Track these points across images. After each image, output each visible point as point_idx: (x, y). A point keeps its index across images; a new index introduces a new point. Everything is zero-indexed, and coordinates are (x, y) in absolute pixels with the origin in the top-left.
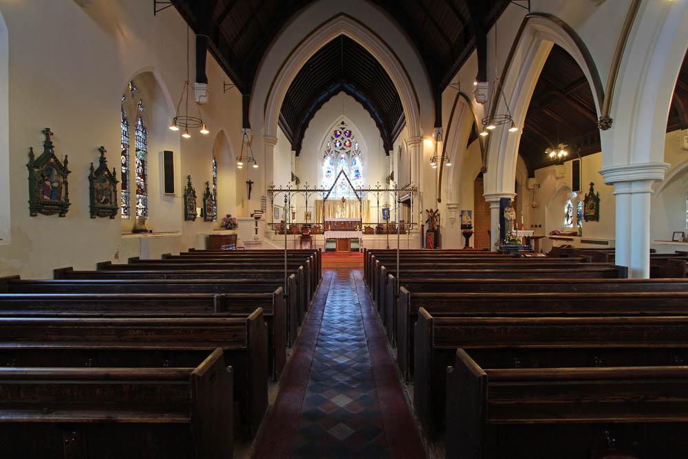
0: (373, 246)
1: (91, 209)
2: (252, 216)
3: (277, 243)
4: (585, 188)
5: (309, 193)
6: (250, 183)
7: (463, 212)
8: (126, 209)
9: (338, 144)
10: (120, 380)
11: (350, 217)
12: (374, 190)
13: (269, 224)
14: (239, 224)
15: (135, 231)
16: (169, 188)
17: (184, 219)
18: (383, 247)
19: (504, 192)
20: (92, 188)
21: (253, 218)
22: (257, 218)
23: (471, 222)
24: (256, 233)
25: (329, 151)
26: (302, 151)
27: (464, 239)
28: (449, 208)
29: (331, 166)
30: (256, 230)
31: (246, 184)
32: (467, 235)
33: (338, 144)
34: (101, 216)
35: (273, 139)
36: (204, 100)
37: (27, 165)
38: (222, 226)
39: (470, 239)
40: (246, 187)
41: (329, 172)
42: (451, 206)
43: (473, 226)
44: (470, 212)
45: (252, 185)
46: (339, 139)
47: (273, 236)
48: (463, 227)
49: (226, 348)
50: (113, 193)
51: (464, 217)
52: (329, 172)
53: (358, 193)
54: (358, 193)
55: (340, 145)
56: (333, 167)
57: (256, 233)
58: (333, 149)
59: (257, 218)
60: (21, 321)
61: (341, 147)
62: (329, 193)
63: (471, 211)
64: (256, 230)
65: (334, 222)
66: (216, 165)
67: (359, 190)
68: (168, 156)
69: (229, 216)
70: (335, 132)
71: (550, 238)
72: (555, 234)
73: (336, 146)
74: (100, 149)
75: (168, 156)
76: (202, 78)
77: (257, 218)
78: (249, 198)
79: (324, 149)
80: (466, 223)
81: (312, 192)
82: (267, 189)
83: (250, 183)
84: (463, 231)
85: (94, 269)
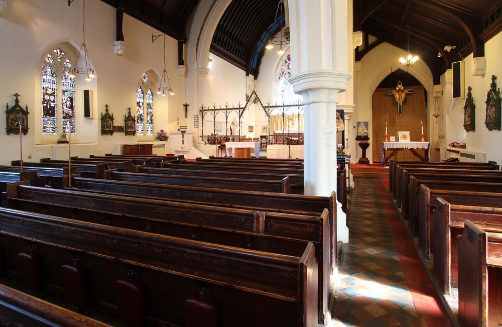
0: (278, 155)
1: (471, 130)
2: (179, 130)
4: (464, 92)
5: (228, 111)
6: (186, 106)
7: (359, 123)
8: (54, 128)
14: (170, 137)
15: (59, 142)
16: (87, 114)
17: (101, 134)
18: (286, 157)
20: (8, 118)
21: (180, 132)
22: (183, 132)
23: (367, 133)
24: (183, 143)
25: (283, 73)
26: (260, 76)
27: (361, 150)
29: (284, 86)
30: (183, 140)
31: (183, 106)
32: (364, 147)
34: (106, 134)
35: (204, 70)
36: (120, 52)
38: (157, 139)
39: (367, 150)
40: (183, 108)
41: (283, 91)
43: (371, 136)
44: (366, 124)
45: (188, 107)
47: (202, 145)
48: (358, 138)
50: (25, 120)
51: (360, 128)
52: (283, 91)
53: (267, 109)
54: (267, 109)
57: (183, 143)
58: (286, 71)
59: (182, 132)
62: (244, 110)
63: (367, 122)
64: (183, 140)
65: (337, 158)
66: (152, 95)
67: (267, 107)
68: (86, 93)
69: (162, 131)
71: (448, 150)
72: (453, 146)
74: (15, 95)
75: (86, 93)
76: (120, 37)
77: (183, 132)
78: (186, 117)
79: (279, 71)
81: (230, 110)
83: (186, 106)
85: (9, 164)
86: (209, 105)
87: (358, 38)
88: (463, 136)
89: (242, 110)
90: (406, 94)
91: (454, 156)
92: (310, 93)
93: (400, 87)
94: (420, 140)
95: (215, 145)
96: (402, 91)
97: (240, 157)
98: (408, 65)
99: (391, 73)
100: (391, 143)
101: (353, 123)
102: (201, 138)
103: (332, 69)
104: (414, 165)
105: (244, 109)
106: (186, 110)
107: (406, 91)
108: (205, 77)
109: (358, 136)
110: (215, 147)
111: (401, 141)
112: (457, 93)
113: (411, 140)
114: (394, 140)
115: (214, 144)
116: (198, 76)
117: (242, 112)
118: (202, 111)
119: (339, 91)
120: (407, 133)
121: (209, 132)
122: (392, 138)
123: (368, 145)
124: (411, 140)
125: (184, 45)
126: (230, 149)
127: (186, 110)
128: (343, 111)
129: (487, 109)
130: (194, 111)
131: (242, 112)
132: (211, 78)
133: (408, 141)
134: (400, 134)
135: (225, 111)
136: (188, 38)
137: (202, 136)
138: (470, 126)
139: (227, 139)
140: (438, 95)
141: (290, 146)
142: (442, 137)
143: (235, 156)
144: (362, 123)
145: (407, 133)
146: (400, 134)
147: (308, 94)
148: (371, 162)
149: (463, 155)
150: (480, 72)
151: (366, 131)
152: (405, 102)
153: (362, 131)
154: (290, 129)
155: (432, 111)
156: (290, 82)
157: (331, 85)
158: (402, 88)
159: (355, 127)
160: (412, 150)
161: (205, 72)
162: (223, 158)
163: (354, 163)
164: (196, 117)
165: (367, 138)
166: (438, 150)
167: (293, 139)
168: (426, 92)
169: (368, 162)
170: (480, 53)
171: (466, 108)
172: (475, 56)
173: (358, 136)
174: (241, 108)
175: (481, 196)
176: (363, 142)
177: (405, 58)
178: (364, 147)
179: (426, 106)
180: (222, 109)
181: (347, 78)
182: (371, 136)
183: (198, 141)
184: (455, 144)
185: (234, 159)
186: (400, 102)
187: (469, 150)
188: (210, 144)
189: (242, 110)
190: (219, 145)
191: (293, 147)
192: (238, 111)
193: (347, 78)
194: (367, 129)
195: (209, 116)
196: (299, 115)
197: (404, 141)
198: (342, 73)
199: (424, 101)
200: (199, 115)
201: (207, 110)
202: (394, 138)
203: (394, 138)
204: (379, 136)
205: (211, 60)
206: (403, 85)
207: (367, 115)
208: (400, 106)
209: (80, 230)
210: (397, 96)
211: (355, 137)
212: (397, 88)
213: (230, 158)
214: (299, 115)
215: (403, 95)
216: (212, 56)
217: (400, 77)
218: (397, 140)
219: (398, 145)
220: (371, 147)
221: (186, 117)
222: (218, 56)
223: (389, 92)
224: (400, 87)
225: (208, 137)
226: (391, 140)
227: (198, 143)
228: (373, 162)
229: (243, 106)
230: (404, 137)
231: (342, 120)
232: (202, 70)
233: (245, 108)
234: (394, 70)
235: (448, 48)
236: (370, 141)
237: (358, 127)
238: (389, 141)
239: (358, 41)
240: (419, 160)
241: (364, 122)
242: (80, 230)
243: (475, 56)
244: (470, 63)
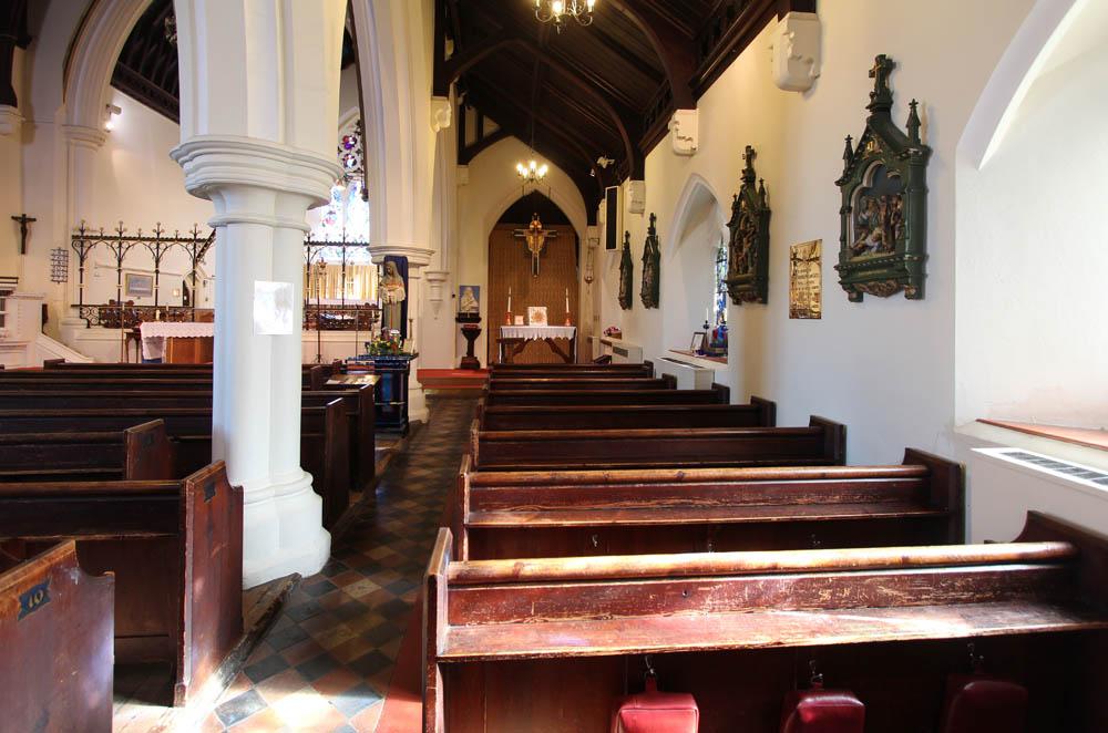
3: (105, 347)
6: (24, 223)
7: (462, 288)
9: (350, 162)
10: (825, 572)
11: (364, 297)
12: (335, 244)
13: (73, 306)
19: (390, 243)
23: (477, 309)
27: (465, 342)
28: (430, 281)
32: (472, 335)
33: (350, 162)
37: (836, 268)
39: (476, 342)
42: (430, 277)
43: (484, 314)
44: (476, 290)
46: (353, 152)
47: (79, 331)
48: (461, 318)
49: (82, 538)
51: (464, 299)
55: (355, 163)
56: (340, 204)
60: (866, 483)
61: (355, 168)
63: (478, 288)
70: (345, 139)
72: (610, 335)
73: (346, 166)
78: (23, 252)
80: (467, 310)
82: (71, 233)
83: (24, 223)
84: (462, 325)
86: (94, 227)
87: (440, 111)
88: (613, 315)
89: (201, 245)
90: (547, 239)
91: (608, 351)
92: (227, 196)
93: (536, 224)
94: (563, 324)
95: (119, 331)
96: (539, 232)
97: (184, 361)
98: (532, 180)
99: (520, 196)
100: (516, 329)
101: (452, 286)
102: (76, 312)
103: (281, 139)
104: (533, 371)
105: (208, 242)
106: (24, 232)
107: (546, 233)
108: (96, 150)
109: (460, 314)
110: (117, 335)
111: (533, 325)
112: (611, 244)
113: (549, 324)
114: (522, 323)
115: (118, 326)
116: (68, 143)
117: (203, 250)
118: (83, 240)
119: (309, 202)
120: (543, 310)
121: (103, 290)
122: (519, 320)
123: (478, 332)
124: (549, 324)
125: (17, 49)
126: (156, 342)
127: (24, 232)
128: (405, 258)
129: (644, 271)
130: (51, 235)
131: (203, 250)
132: (118, 157)
133: (544, 324)
134: (532, 311)
135: (154, 245)
136: (37, 38)
137: (81, 306)
138: (626, 302)
139: (149, 314)
140: (593, 244)
141: (322, 332)
142: (596, 318)
143: (168, 360)
144: (469, 289)
145: (543, 310)
146: (532, 311)
147: (223, 200)
148: (484, 365)
149: (617, 350)
150: (637, 207)
151: (475, 304)
152: (543, 253)
153: (468, 304)
154: (345, 297)
155: (584, 273)
156: (177, 160)
157: (281, 182)
158: (540, 226)
159: (454, 296)
160: (548, 340)
161: (101, 138)
162: (135, 366)
163: (452, 368)
164: (60, 258)
165: (476, 318)
166: (590, 340)
167: (328, 316)
168: (577, 238)
169: (478, 364)
170: (639, 175)
171: (621, 268)
172: (631, 179)
173: (460, 314)
174: (200, 241)
175: (572, 439)
176: (468, 324)
177: (526, 165)
178: (472, 335)
179: (577, 265)
180: (144, 239)
181: (333, 173)
182: (484, 314)
183: (62, 317)
184: (613, 332)
185: (168, 366)
186: (536, 252)
187: (624, 343)
188: (106, 326)
189: (201, 245)
190: (131, 331)
191: (327, 335)
192: (191, 246)
193: (333, 173)
194: (478, 300)
195: (102, 254)
196: (344, 265)
197: (535, 325)
198: (315, 156)
199: (575, 256)
200: (70, 249)
201: (96, 238)
202: (521, 318)
203: (521, 318)
204: (498, 316)
205: (118, 111)
206: (542, 222)
207: (476, 272)
208: (536, 259)
209: (123, 499)
210: (531, 240)
211: (455, 316)
212: (532, 226)
213: (155, 364)
214: (344, 265)
215: (541, 240)
216: (121, 100)
217: (531, 207)
218: (526, 322)
219: (526, 333)
220: (483, 338)
221: (23, 252)
222: (146, 104)
223: (519, 233)
224: (536, 224)
225: (102, 308)
226: (517, 323)
227: (65, 324)
228: (488, 364)
229: (205, 235)
230: (538, 317)
231: (399, 279)
232: (82, 130)
233: (210, 239)
234: (527, 192)
235: (603, 162)
236: (483, 325)
237: (461, 295)
238: (513, 324)
239: (442, 118)
240: (560, 360)
241: (472, 287)
242: (123, 499)
243: (631, 179)
244: (627, 190)
